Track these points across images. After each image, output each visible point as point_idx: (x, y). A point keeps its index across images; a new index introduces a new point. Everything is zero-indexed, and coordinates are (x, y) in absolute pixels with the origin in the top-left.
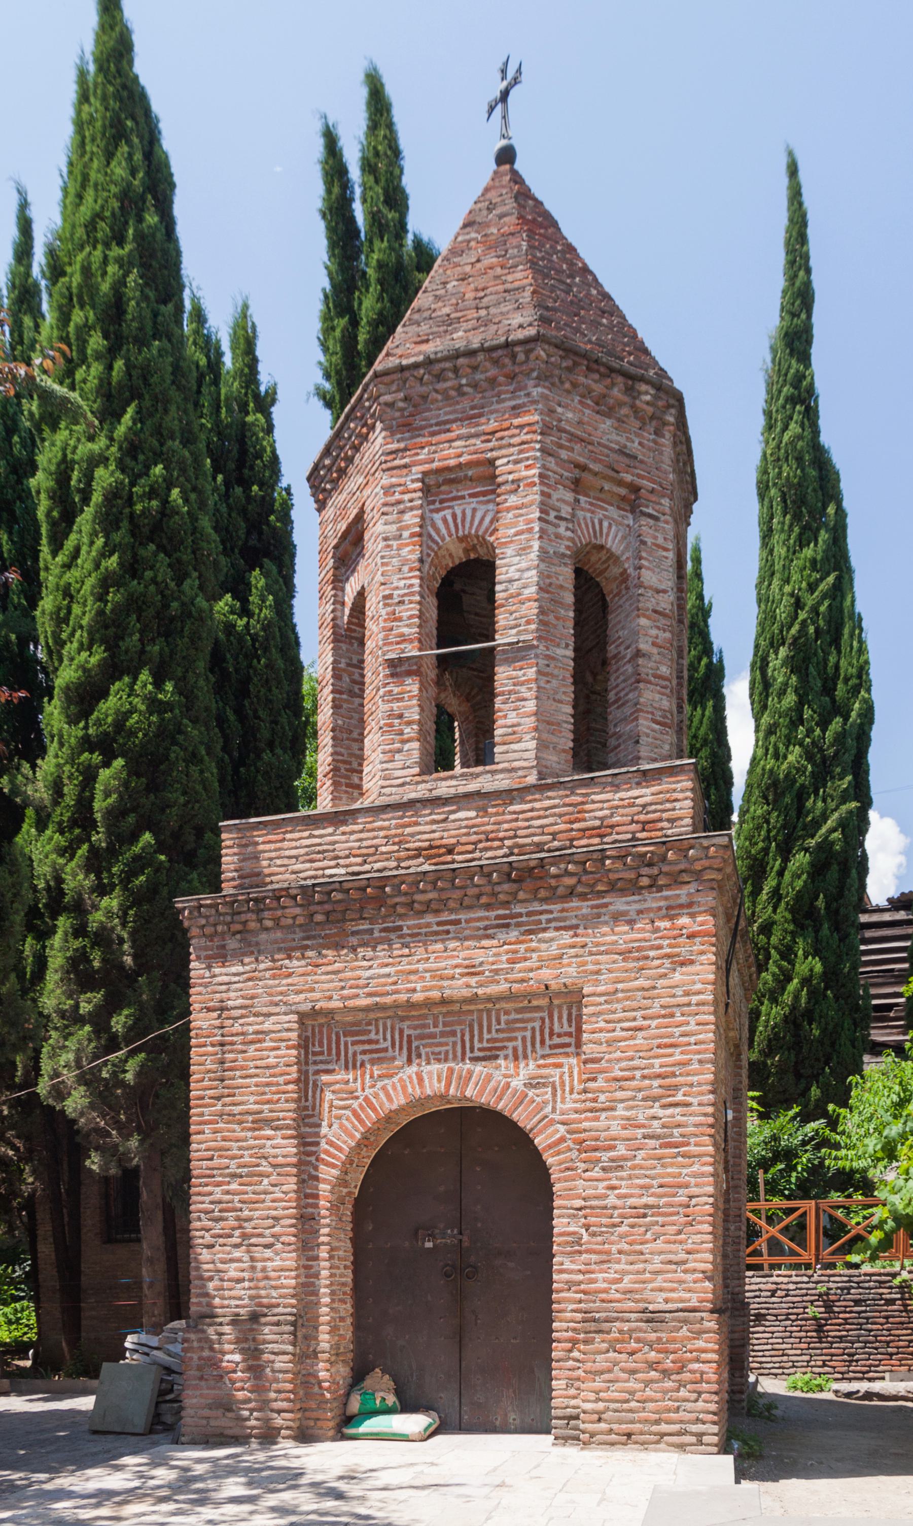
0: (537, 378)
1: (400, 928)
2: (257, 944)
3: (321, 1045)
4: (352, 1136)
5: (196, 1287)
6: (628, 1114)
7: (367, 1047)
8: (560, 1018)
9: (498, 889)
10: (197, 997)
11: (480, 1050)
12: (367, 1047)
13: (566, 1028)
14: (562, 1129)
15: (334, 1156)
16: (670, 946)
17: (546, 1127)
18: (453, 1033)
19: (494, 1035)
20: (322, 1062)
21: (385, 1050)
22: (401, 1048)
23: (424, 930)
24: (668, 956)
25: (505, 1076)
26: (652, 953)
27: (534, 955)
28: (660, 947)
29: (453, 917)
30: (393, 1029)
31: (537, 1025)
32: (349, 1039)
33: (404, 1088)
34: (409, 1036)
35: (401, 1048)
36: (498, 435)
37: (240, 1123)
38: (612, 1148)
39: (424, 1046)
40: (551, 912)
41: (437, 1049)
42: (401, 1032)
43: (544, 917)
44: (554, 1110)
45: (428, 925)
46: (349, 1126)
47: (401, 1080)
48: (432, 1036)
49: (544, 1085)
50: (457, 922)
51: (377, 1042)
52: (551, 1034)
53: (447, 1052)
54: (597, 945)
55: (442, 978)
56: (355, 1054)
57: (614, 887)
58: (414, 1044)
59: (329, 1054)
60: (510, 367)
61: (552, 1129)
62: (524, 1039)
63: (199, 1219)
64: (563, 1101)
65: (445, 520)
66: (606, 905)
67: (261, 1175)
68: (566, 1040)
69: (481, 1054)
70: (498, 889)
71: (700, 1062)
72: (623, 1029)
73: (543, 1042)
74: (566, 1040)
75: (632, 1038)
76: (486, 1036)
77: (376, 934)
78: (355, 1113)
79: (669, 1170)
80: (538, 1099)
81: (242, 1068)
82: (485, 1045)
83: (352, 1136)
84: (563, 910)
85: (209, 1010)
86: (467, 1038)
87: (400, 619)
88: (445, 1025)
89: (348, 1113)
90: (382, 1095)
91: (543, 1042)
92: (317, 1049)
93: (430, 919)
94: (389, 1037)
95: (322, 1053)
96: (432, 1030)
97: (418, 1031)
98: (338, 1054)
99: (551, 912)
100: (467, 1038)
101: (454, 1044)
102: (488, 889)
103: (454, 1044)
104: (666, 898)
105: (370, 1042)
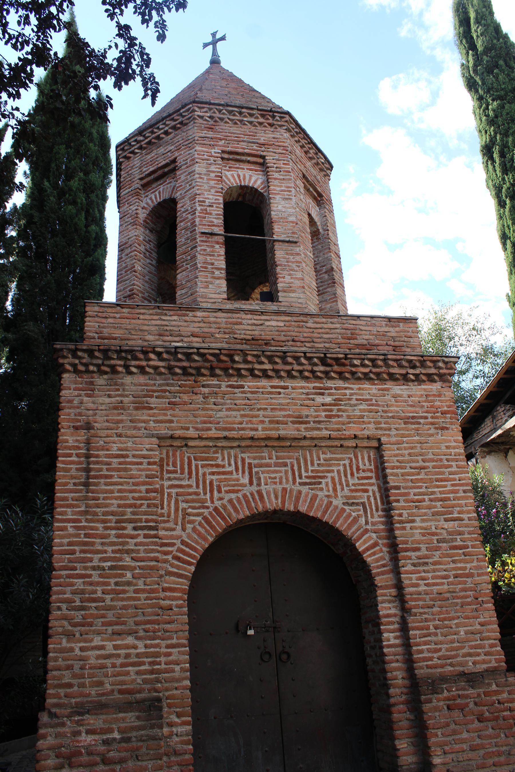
0: (286, 129)
1: (242, 387)
2: (122, 384)
3: (174, 465)
4: (205, 539)
5: (54, 678)
6: (424, 525)
7: (215, 470)
8: (363, 459)
9: (315, 368)
10: (66, 417)
11: (307, 477)
12: (215, 470)
13: (368, 466)
14: (374, 535)
15: (190, 555)
16: (432, 417)
17: (362, 535)
18: (286, 465)
19: (316, 468)
20: (175, 478)
21: (231, 473)
22: (243, 472)
23: (261, 390)
24: (432, 424)
25: (328, 496)
26: (422, 421)
27: (344, 414)
28: (426, 418)
29: (282, 384)
30: (236, 457)
31: (347, 462)
32: (200, 463)
33: (248, 502)
34: (250, 464)
35: (243, 472)
36: (266, 146)
37: (104, 521)
38: (418, 549)
39: (263, 472)
40: (352, 389)
41: (273, 475)
42: (243, 460)
43: (348, 392)
44: (367, 523)
45: (264, 387)
46: (202, 531)
47: (245, 496)
48: (268, 465)
49: (357, 504)
50: (286, 388)
51: (223, 466)
52: (358, 469)
53: (281, 478)
54: (386, 412)
55: (278, 422)
56: (204, 475)
57: (392, 377)
58: (255, 470)
59: (182, 473)
60: (271, 121)
61: (368, 535)
62: (339, 472)
63: (59, 608)
64: (372, 516)
65: (233, 176)
66: (388, 390)
67: (123, 568)
68: (369, 474)
69: (308, 481)
70: (315, 368)
71: (465, 491)
72: (411, 468)
73: (352, 474)
74: (369, 474)
75: (418, 474)
76: (310, 468)
77: (224, 388)
78: (205, 518)
79: (459, 565)
80: (354, 514)
81: (106, 477)
82: (310, 474)
83: (205, 539)
84: (360, 389)
85: (76, 428)
86: (296, 468)
87: (211, 214)
88: (277, 458)
89: (199, 519)
90: (229, 507)
91: (352, 474)
92: (171, 468)
93: (264, 382)
94: (233, 463)
95: (175, 472)
96: (268, 461)
97: (256, 462)
98: (190, 473)
99: (352, 389)
100: (296, 468)
101: (286, 472)
102: (309, 368)
103: (286, 472)
104: (425, 390)
105: (218, 466)
